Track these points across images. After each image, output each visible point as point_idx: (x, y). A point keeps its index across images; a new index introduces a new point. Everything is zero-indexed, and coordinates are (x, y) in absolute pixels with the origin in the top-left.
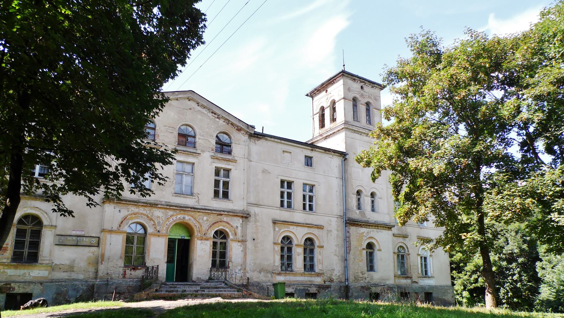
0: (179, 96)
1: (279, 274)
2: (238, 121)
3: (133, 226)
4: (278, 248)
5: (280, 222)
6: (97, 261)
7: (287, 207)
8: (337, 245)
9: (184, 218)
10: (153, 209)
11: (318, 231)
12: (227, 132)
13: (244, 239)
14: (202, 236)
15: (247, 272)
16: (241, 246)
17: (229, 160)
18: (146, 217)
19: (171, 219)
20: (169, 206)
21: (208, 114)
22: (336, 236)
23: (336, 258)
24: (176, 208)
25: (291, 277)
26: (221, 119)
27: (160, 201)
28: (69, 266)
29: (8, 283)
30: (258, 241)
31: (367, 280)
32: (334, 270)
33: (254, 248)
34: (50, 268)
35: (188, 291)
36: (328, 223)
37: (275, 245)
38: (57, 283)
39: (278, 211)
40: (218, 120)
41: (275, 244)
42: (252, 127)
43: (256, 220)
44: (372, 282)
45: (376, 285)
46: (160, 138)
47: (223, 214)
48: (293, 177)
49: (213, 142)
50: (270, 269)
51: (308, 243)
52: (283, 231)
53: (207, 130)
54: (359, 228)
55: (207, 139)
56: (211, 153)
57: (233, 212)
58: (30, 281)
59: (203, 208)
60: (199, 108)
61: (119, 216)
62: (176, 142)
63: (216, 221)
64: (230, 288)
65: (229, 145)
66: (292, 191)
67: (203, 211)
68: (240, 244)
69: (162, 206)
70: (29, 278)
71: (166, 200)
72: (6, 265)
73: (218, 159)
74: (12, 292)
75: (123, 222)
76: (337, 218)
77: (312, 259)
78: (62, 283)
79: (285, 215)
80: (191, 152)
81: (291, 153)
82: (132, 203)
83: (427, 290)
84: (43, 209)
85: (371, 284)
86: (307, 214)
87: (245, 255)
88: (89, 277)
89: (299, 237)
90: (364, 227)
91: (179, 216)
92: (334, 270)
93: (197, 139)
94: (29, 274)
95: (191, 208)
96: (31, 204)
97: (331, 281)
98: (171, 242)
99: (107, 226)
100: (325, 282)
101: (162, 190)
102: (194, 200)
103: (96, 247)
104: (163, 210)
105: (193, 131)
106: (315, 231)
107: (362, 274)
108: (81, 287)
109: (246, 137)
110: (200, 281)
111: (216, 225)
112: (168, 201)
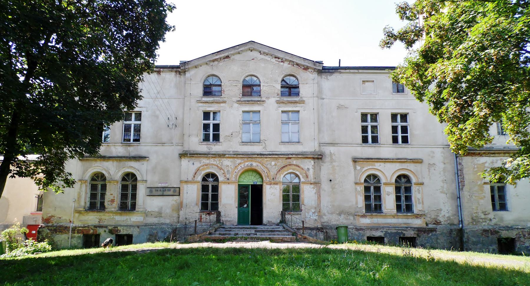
0: (239, 50)
1: (364, 216)
2: (302, 61)
3: (288, 177)
4: (361, 189)
5: (362, 160)
6: (180, 206)
7: (372, 143)
8: (444, 181)
9: (252, 165)
10: (222, 159)
11: (415, 166)
12: (293, 73)
13: (317, 181)
14: (270, 180)
15: (325, 215)
16: (314, 188)
17: (296, 102)
18: (216, 167)
19: (240, 167)
20: (236, 155)
21: (272, 60)
22: (442, 169)
23: (444, 196)
24: (243, 156)
25: (379, 219)
26: (286, 62)
27: (228, 151)
28: (158, 212)
29: (116, 227)
30: (336, 182)
31: (493, 222)
32: (441, 210)
33: (331, 190)
34: (144, 214)
35: (240, 234)
36: (429, 155)
37: (357, 185)
38: (149, 227)
39: (359, 149)
40: (282, 63)
41: (356, 183)
42: (320, 63)
43: (332, 161)
44: (502, 224)
45: (508, 227)
46: (225, 93)
47: (291, 158)
48: (377, 107)
49: (278, 86)
50: (352, 211)
51: (403, 180)
52: (366, 170)
53: (271, 76)
54: (476, 157)
55: (272, 85)
56: (277, 98)
57: (302, 155)
58: (131, 225)
59: (271, 153)
60: (262, 56)
61: (193, 168)
62: (241, 94)
63: (284, 165)
64: (287, 232)
65: (297, 87)
66: (378, 124)
67: (270, 156)
68: (312, 186)
69: (229, 156)
70: (130, 222)
71: (234, 150)
72: (114, 213)
73: (284, 103)
74: (119, 233)
75: (197, 173)
76: (443, 148)
77: (408, 198)
78: (153, 226)
79: (369, 151)
80: (255, 101)
81: (373, 81)
82: (202, 156)
83: (504, 234)
84: (137, 168)
85: (500, 227)
86: (398, 148)
87: (319, 197)
88: (174, 222)
89: (389, 175)
90: (485, 156)
91: (247, 164)
92: (441, 210)
93: (223, 87)
94: (130, 220)
95: (258, 155)
96: (128, 165)
97: (437, 223)
98: (242, 188)
99: (184, 178)
100: (427, 224)
101: (229, 141)
102: (261, 147)
103: (178, 196)
104: (232, 160)
105: (258, 80)
106: (411, 167)
107: (485, 215)
108: (167, 230)
109: (315, 75)
110: (271, 224)
111: (285, 169)
112: (236, 150)
